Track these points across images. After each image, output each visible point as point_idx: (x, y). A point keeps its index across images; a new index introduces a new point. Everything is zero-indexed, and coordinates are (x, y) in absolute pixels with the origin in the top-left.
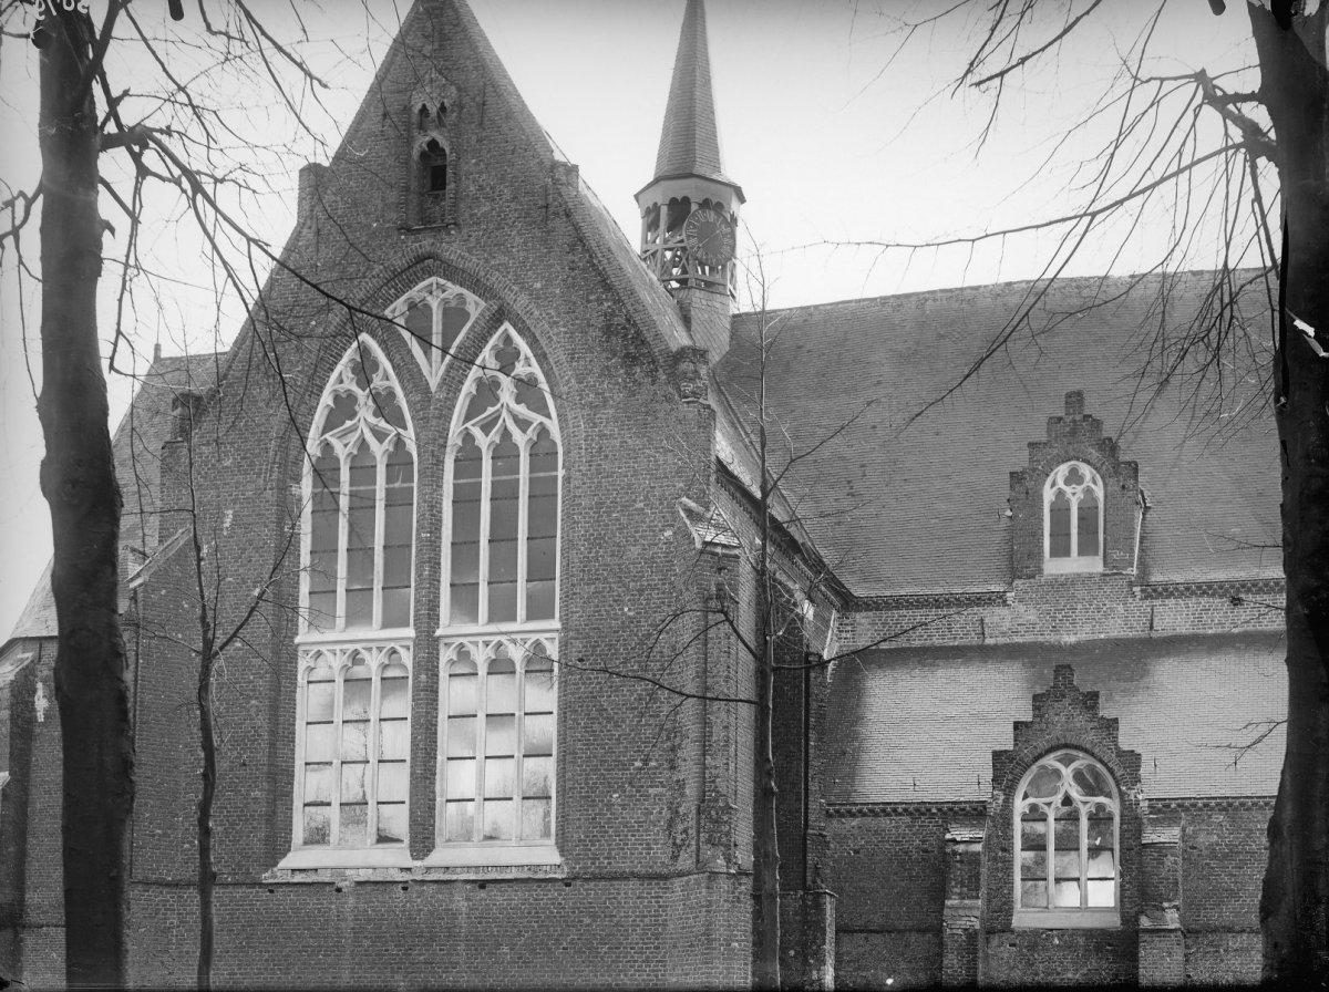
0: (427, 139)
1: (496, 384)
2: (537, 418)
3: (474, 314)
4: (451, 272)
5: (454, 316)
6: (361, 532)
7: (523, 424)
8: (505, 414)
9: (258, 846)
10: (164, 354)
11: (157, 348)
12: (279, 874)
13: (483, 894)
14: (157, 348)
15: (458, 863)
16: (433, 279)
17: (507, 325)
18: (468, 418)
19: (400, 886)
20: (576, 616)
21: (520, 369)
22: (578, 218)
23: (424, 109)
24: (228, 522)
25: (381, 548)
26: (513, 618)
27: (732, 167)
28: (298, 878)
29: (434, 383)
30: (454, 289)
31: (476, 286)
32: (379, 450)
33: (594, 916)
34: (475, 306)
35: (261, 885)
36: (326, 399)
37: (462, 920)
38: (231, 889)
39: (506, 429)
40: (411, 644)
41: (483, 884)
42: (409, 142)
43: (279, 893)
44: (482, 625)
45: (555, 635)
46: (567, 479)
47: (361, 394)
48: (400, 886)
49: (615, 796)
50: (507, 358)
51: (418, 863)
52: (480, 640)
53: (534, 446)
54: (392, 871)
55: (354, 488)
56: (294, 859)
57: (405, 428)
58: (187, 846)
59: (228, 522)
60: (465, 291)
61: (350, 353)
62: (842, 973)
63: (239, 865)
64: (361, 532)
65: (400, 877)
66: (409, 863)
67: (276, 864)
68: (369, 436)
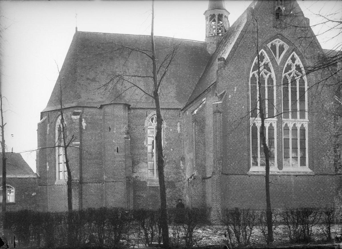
0: (278, 7)
1: (291, 65)
4: (283, 38)
6: (262, 95)
9: (246, 167)
10: (78, 30)
11: (76, 28)
12: (250, 173)
13: (297, 178)
14: (76, 28)
15: (290, 171)
16: (278, 39)
17: (294, 52)
19: (279, 176)
20: (314, 119)
21: (297, 62)
24: (235, 90)
28: (255, 173)
29: (279, 63)
30: (282, 42)
31: (289, 43)
32: (266, 77)
33: (320, 183)
34: (286, 47)
35: (247, 175)
37: (293, 183)
38: (240, 176)
40: (276, 122)
41: (297, 176)
42: (275, 7)
43: (251, 177)
45: (307, 122)
46: (248, 90)
48: (279, 176)
49: (323, 158)
50: (293, 60)
51: (281, 171)
53: (268, 79)
54: (275, 173)
55: (268, 85)
58: (229, 166)
59: (235, 90)
63: (242, 171)
65: (277, 174)
66: (279, 171)
67: (249, 171)
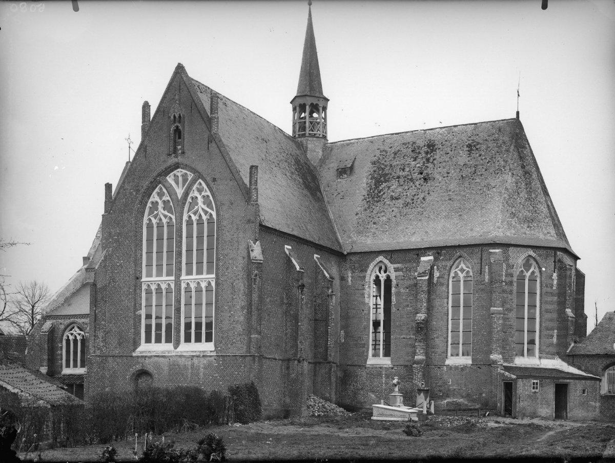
2: (169, 215)
3: (190, 178)
5: (185, 177)
6: (160, 247)
7: (206, 212)
8: (160, 213)
18: (149, 215)
22: (68, 294)
23: (175, 117)
25: (184, 305)
26: (202, 274)
27: (326, 93)
30: (184, 171)
36: (149, 205)
39: (200, 214)
44: (194, 276)
47: (160, 202)
52: (193, 281)
56: (140, 349)
57: (213, 211)
60: (187, 172)
61: (157, 190)
62: (126, 186)
64: (160, 247)
68: (203, 214)
